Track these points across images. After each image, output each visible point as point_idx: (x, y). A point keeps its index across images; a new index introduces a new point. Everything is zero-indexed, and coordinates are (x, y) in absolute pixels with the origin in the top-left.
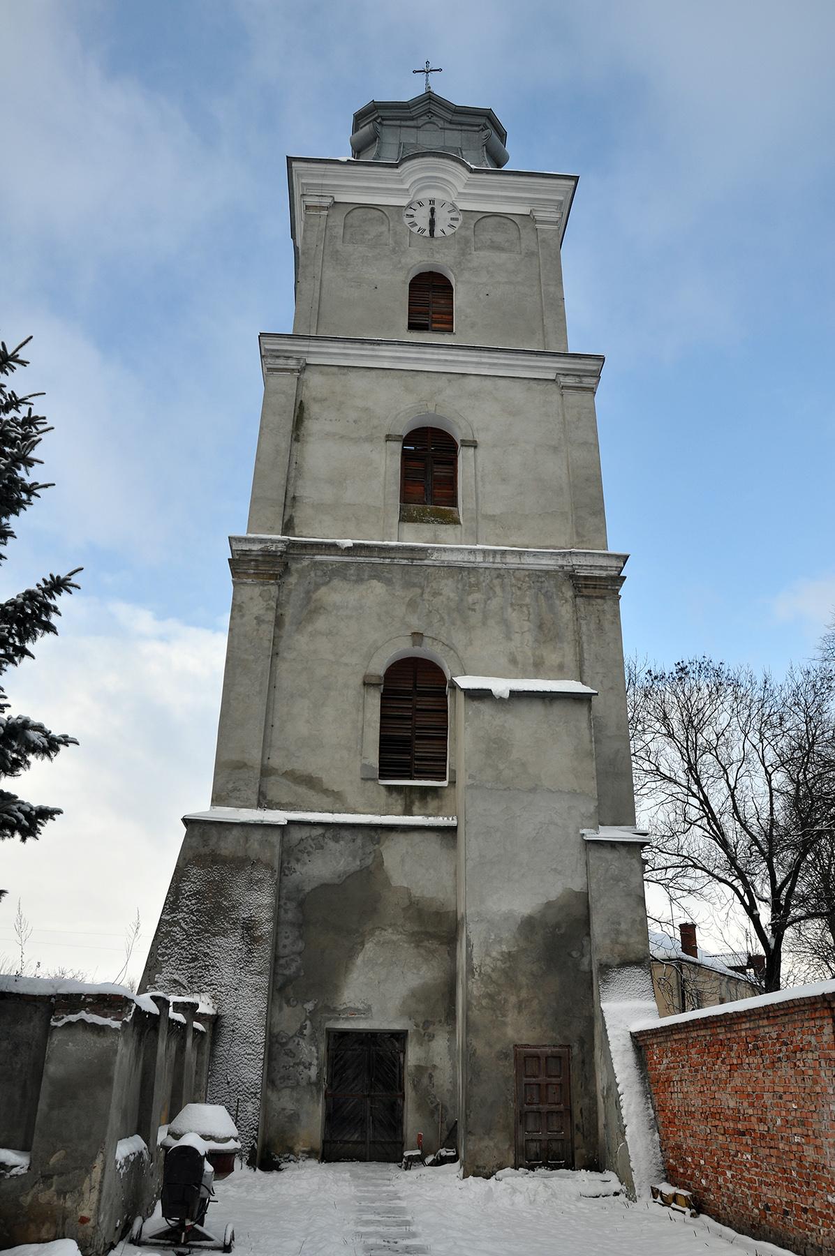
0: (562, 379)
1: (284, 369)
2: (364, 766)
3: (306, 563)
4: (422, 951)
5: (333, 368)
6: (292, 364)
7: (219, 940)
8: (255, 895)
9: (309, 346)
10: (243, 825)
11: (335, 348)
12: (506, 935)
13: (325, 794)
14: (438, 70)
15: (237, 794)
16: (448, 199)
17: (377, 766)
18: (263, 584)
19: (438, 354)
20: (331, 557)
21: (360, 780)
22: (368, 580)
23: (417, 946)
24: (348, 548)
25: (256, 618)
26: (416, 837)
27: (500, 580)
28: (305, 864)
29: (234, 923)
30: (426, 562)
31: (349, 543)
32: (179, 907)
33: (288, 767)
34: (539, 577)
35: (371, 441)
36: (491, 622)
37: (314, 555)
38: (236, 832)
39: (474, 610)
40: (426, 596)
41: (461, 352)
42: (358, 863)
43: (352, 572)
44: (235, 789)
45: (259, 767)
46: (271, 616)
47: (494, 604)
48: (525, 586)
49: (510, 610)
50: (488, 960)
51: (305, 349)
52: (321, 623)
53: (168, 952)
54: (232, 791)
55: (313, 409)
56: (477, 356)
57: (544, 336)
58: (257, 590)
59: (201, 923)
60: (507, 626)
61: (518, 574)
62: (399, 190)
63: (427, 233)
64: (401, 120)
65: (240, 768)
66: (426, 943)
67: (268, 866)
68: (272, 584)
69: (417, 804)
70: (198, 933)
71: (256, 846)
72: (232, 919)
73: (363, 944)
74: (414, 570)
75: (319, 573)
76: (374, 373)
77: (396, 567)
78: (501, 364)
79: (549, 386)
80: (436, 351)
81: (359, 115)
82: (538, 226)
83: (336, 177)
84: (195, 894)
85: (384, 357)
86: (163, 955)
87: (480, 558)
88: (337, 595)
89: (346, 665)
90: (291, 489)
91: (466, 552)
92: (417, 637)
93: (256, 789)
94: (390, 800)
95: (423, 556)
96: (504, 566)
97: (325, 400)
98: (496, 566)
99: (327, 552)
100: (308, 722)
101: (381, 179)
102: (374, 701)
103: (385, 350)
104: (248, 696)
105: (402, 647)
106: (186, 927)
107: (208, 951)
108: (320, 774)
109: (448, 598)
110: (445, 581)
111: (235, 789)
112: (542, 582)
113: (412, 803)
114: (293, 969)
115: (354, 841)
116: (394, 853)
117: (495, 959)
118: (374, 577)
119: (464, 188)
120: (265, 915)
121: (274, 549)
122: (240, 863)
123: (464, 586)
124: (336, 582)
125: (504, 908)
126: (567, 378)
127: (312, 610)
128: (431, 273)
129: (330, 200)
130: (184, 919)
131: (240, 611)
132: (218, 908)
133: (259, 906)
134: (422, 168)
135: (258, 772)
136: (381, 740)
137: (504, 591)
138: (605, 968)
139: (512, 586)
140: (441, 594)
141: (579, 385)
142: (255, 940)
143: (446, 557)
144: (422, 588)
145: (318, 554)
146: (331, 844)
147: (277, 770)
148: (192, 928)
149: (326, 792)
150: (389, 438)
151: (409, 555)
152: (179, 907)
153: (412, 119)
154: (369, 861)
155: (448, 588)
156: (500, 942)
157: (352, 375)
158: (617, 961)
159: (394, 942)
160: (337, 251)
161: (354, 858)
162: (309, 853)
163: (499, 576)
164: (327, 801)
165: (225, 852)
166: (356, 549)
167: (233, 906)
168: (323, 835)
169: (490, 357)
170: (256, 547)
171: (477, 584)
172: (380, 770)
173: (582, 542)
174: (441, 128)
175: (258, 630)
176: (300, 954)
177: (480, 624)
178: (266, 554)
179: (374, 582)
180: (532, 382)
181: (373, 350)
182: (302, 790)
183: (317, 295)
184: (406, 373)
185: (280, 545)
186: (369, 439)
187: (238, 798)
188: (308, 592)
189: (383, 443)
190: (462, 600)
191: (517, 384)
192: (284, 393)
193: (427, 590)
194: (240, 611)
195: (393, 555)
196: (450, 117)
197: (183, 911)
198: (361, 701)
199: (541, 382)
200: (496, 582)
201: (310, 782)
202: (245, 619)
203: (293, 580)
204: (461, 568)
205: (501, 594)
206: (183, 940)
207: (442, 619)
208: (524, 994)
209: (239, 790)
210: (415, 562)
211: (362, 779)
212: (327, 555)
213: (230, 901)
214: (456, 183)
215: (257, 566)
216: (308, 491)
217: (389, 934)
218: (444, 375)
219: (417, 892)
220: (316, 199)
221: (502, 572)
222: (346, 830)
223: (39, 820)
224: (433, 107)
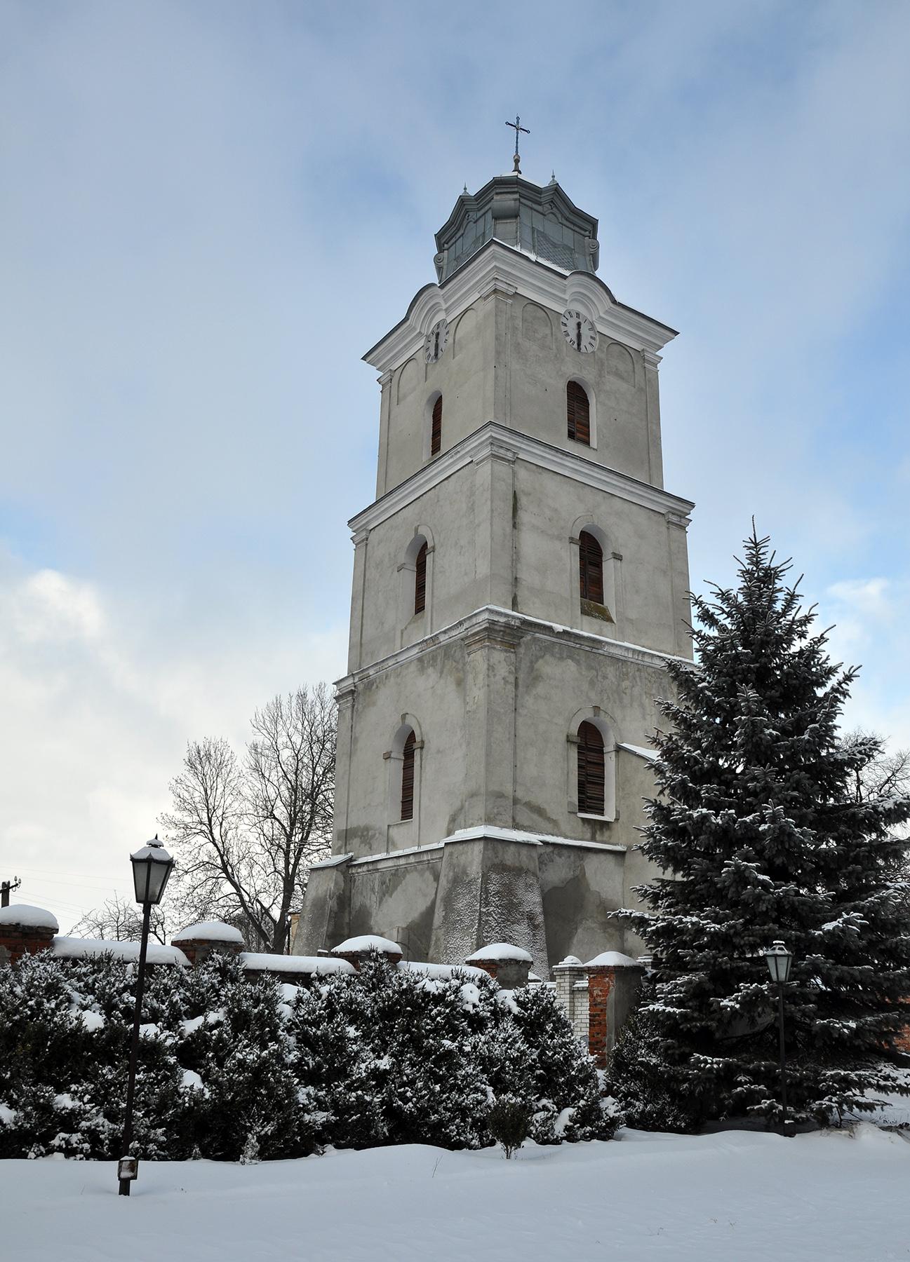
1: (503, 458)
2: (570, 803)
5: (532, 465)
6: (509, 455)
7: (516, 927)
9: (522, 443)
11: (538, 450)
13: (548, 820)
14: (509, 124)
15: (499, 817)
17: (577, 803)
20: (546, 636)
21: (567, 813)
22: (566, 659)
26: (602, 857)
27: (639, 673)
28: (544, 872)
29: (522, 915)
30: (600, 651)
31: (559, 628)
33: (527, 799)
34: (660, 674)
35: (561, 540)
36: (635, 705)
37: (535, 633)
39: (625, 693)
41: (615, 477)
42: (572, 873)
43: (556, 650)
44: (499, 814)
46: (512, 679)
47: (636, 690)
48: (653, 680)
51: (519, 445)
52: (540, 689)
53: (489, 935)
54: (497, 814)
55: (523, 501)
56: (623, 483)
57: (650, 469)
58: (502, 655)
61: (650, 670)
62: (561, 298)
63: (575, 346)
65: (500, 797)
66: (609, 930)
69: (598, 832)
71: (525, 859)
72: (521, 912)
73: (576, 929)
74: (592, 656)
76: (559, 477)
79: (660, 519)
80: (600, 472)
81: (498, 181)
83: (521, 270)
84: (497, 893)
86: (487, 937)
88: (550, 667)
94: (585, 829)
95: (599, 647)
96: (642, 663)
98: (638, 662)
100: (536, 765)
103: (570, 462)
104: (502, 741)
105: (588, 715)
107: (511, 934)
108: (545, 806)
110: (609, 668)
111: (499, 814)
112: (661, 679)
113: (596, 832)
116: (592, 865)
119: (604, 314)
121: (513, 623)
123: (620, 673)
127: (536, 678)
130: (494, 911)
131: (493, 671)
132: (511, 902)
133: (534, 903)
136: (579, 784)
137: (641, 681)
139: (646, 678)
141: (679, 523)
142: (536, 927)
143: (613, 651)
144: (597, 671)
145: (538, 633)
146: (558, 858)
147: (520, 800)
149: (549, 819)
151: (591, 645)
152: (489, 902)
154: (578, 872)
155: (611, 672)
157: (546, 475)
159: (593, 929)
160: (519, 344)
161: (570, 869)
163: (639, 670)
164: (549, 826)
165: (508, 863)
169: (631, 486)
170: (502, 620)
171: (627, 674)
172: (579, 806)
173: (680, 651)
174: (560, 223)
175: (505, 689)
177: (629, 705)
180: (651, 512)
181: (562, 459)
182: (535, 817)
185: (517, 621)
186: (559, 538)
187: (501, 820)
188: (531, 662)
189: (568, 544)
190: (619, 685)
191: (643, 511)
192: (504, 480)
194: (493, 671)
195: (582, 643)
196: (568, 215)
197: (492, 906)
198: (566, 754)
199: (656, 514)
200: (637, 674)
201: (539, 811)
202: (497, 678)
203: (522, 650)
205: (639, 684)
206: (496, 926)
209: (501, 814)
210: (594, 650)
211: (569, 812)
212: (543, 634)
213: (518, 899)
214: (599, 308)
217: (589, 923)
218: (601, 492)
219: (603, 895)
220: (505, 286)
222: (565, 849)
223: (774, 942)
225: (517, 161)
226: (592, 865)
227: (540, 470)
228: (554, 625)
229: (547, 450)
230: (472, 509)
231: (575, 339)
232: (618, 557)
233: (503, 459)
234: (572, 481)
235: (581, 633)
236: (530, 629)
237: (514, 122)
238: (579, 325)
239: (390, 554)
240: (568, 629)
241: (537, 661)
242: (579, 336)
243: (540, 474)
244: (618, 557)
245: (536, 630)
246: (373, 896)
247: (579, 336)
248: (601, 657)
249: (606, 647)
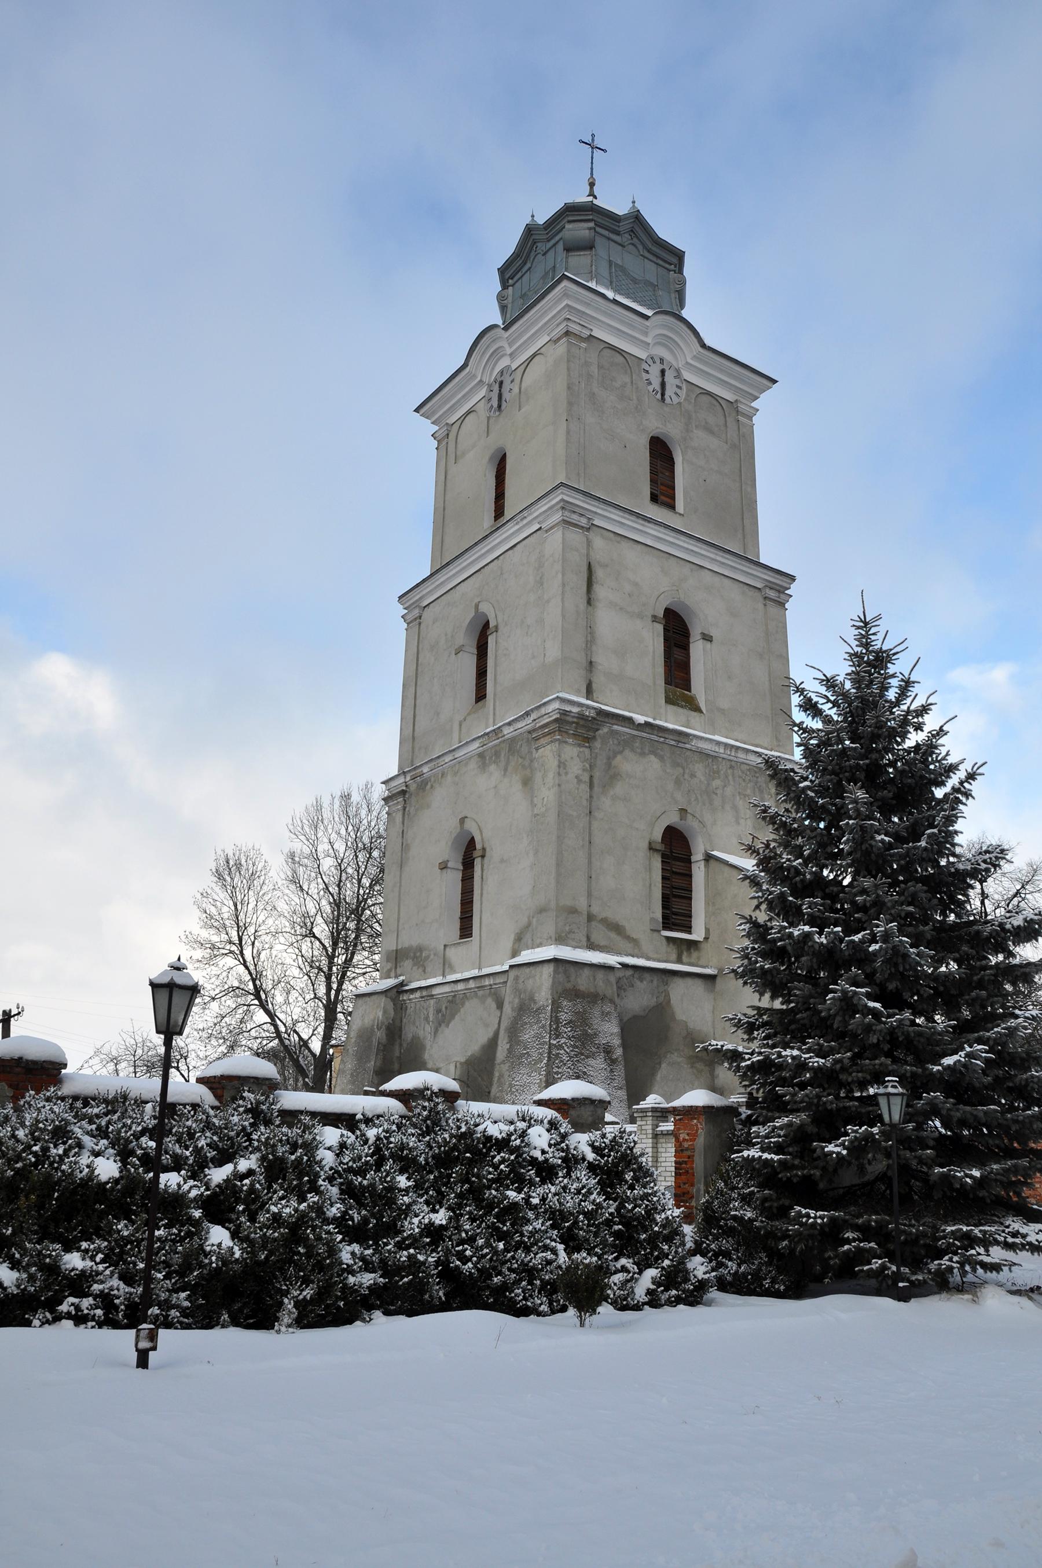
0: (767, 590)
2: (652, 920)
3: (606, 730)
4: (695, 1071)
6: (583, 521)
8: (608, 1025)
9: (598, 507)
10: (592, 966)
11: (615, 515)
15: (572, 936)
16: (674, 363)
17: (661, 920)
18: (579, 745)
19: (688, 543)
23: (692, 1067)
24: (639, 724)
25: (577, 777)
26: (689, 981)
29: (598, 1048)
30: (687, 746)
31: (640, 719)
32: (560, 1034)
33: (603, 915)
36: (728, 807)
39: (716, 794)
40: (686, 776)
41: (705, 547)
43: (637, 744)
44: (571, 932)
46: (586, 778)
47: (729, 790)
49: (738, 798)
52: (619, 789)
53: (560, 1070)
55: (599, 573)
59: (577, 1047)
60: (737, 812)
62: (642, 341)
63: (659, 396)
68: (586, 747)
70: (576, 1055)
71: (601, 983)
73: (660, 1064)
75: (616, 742)
76: (640, 546)
77: (666, 746)
78: (729, 565)
82: (740, 418)
83: (597, 309)
84: (568, 1023)
85: (649, 534)
86: (557, 1073)
87: (722, 751)
88: (629, 764)
89: (637, 829)
92: (683, 812)
93: (585, 933)
94: (669, 950)
95: (685, 740)
96: (735, 759)
97: (607, 566)
99: (623, 724)
101: (632, 326)
102: (657, 863)
103: (652, 529)
105: (672, 818)
106: (568, 1050)
109: (700, 781)
110: (697, 765)
111: (571, 932)
115: (652, 981)
119: (692, 359)
120: (616, 1042)
121: (587, 714)
122: (594, 998)
124: (627, 752)
126: (771, 591)
128: (665, 443)
130: (565, 1043)
132: (585, 1034)
134: (666, 326)
135: (585, 917)
137: (734, 781)
140: (695, 776)
143: (702, 745)
146: (638, 983)
148: (572, 1051)
149: (628, 938)
151: (677, 738)
154: (661, 999)
155: (699, 769)
157: (625, 544)
162: (625, 990)
163: (731, 767)
164: (629, 946)
165: (582, 988)
167: (595, 1034)
168: (633, 976)
170: (575, 710)
171: (718, 772)
172: (663, 923)
178: (581, 716)
179: (652, 757)
181: (643, 525)
182: (613, 935)
186: (640, 616)
188: (609, 758)
191: (736, 585)
194: (565, 769)
195: (667, 736)
197: (563, 1037)
199: (751, 589)
200: (730, 771)
201: (617, 928)
203: (597, 744)
204: (708, 755)
207: (697, 799)
209: (574, 932)
210: (681, 745)
211: (652, 930)
215: (576, 728)
219: (691, 1025)
220: (578, 328)
221: (733, 763)
225: (592, 185)
226: (678, 990)
229: (626, 516)
230: (540, 582)
231: (658, 388)
232: (707, 638)
233: (576, 525)
236: (606, 720)
237: (588, 139)
238: (663, 372)
239: (446, 635)
240: (651, 720)
242: (663, 385)
243: (618, 542)
244: (707, 638)
245: (614, 721)
246: (427, 1025)
247: (663, 385)
248: (688, 753)
249: (694, 741)
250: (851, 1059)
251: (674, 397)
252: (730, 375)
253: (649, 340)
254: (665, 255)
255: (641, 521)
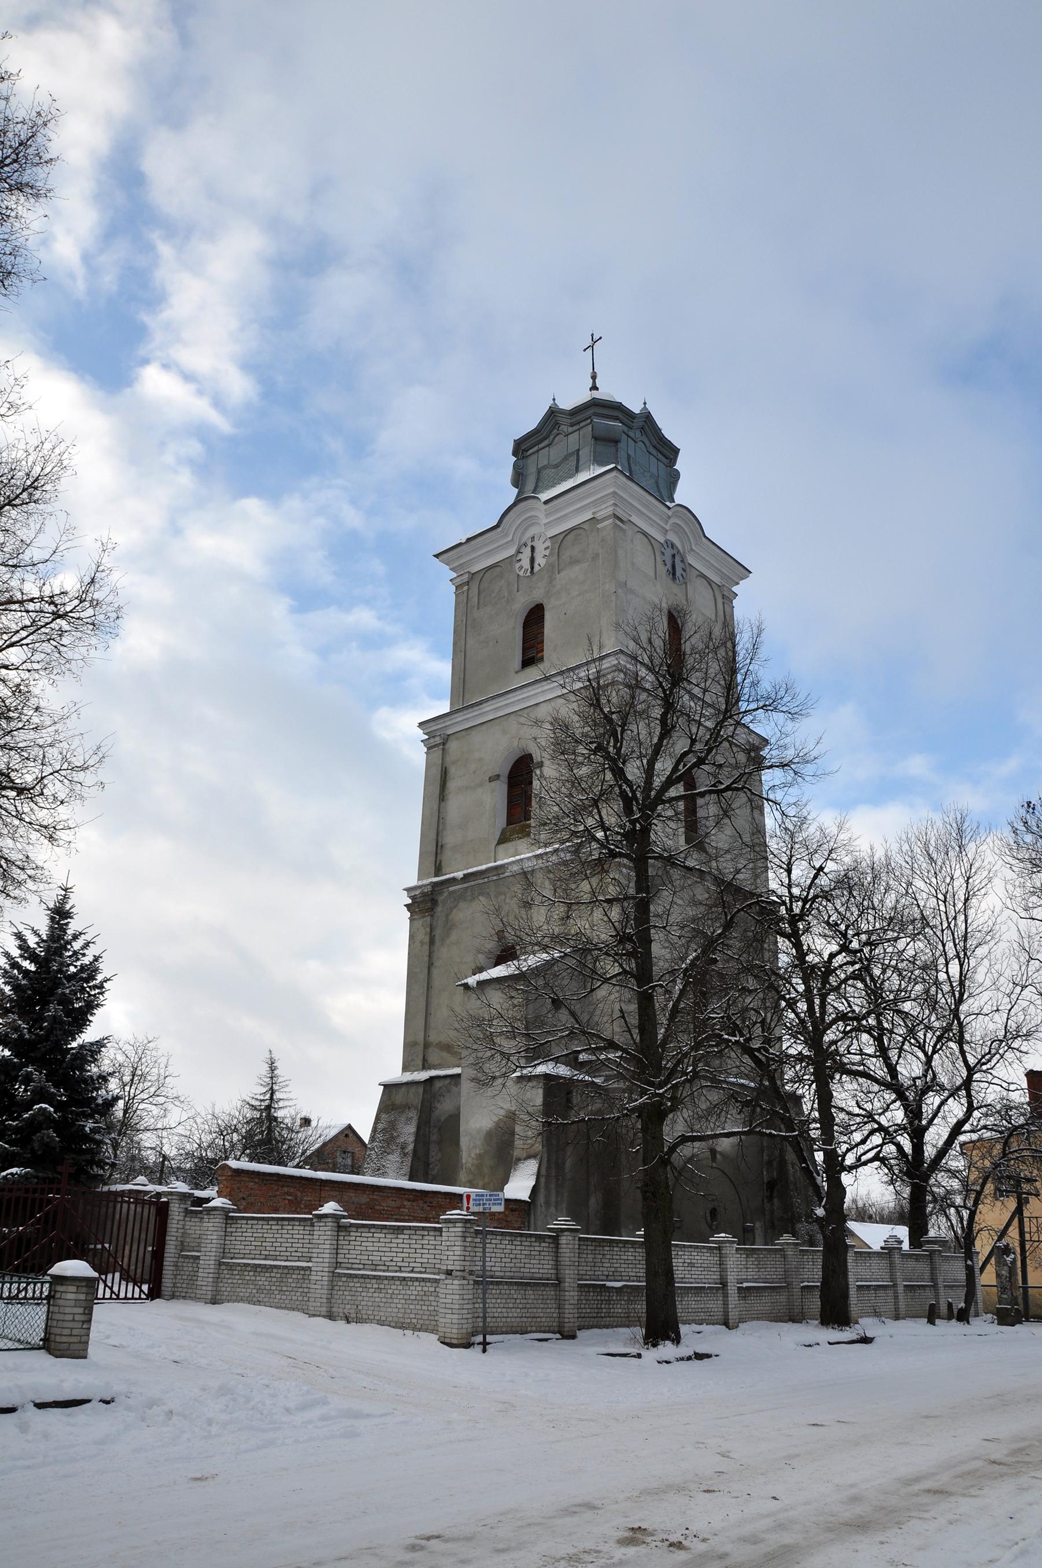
3: (445, 894)
7: (390, 1157)
12: (478, 1143)
31: (459, 875)
38: (403, 1089)
40: (507, 901)
41: (530, 688)
45: (422, 1043)
50: (470, 1159)
51: (443, 725)
55: (452, 771)
59: (384, 1147)
63: (528, 574)
64: (538, 444)
67: (416, 1108)
76: (485, 726)
90: (440, 840)
91: (526, 861)
95: (503, 871)
114: (436, 1170)
117: (473, 1159)
118: (480, 894)
120: (412, 1139)
125: (478, 1126)
127: (449, 926)
129: (467, 576)
138: (519, 1160)
150: (491, 779)
151: (495, 873)
153: (545, 439)
156: (475, 1148)
158: (525, 1156)
165: (398, 1102)
166: (467, 877)
168: (450, 1083)
176: (439, 1161)
182: (445, 1054)
183: (463, 666)
184: (502, 718)
186: (481, 785)
193: (508, 895)
203: (439, 909)
208: (486, 1180)
210: (502, 876)
216: (450, 839)
224: (558, 418)
225: (594, 377)
227: (469, 731)
228: (455, 875)
229: (465, 712)
231: (670, 569)
234: (498, 720)
235: (479, 868)
238: (674, 556)
240: (465, 872)
241: (451, 911)
245: (448, 885)
249: (510, 868)
250: (227, 1158)
251: (681, 577)
252: (581, 500)
253: (667, 528)
254: (582, 416)
255: (476, 708)
